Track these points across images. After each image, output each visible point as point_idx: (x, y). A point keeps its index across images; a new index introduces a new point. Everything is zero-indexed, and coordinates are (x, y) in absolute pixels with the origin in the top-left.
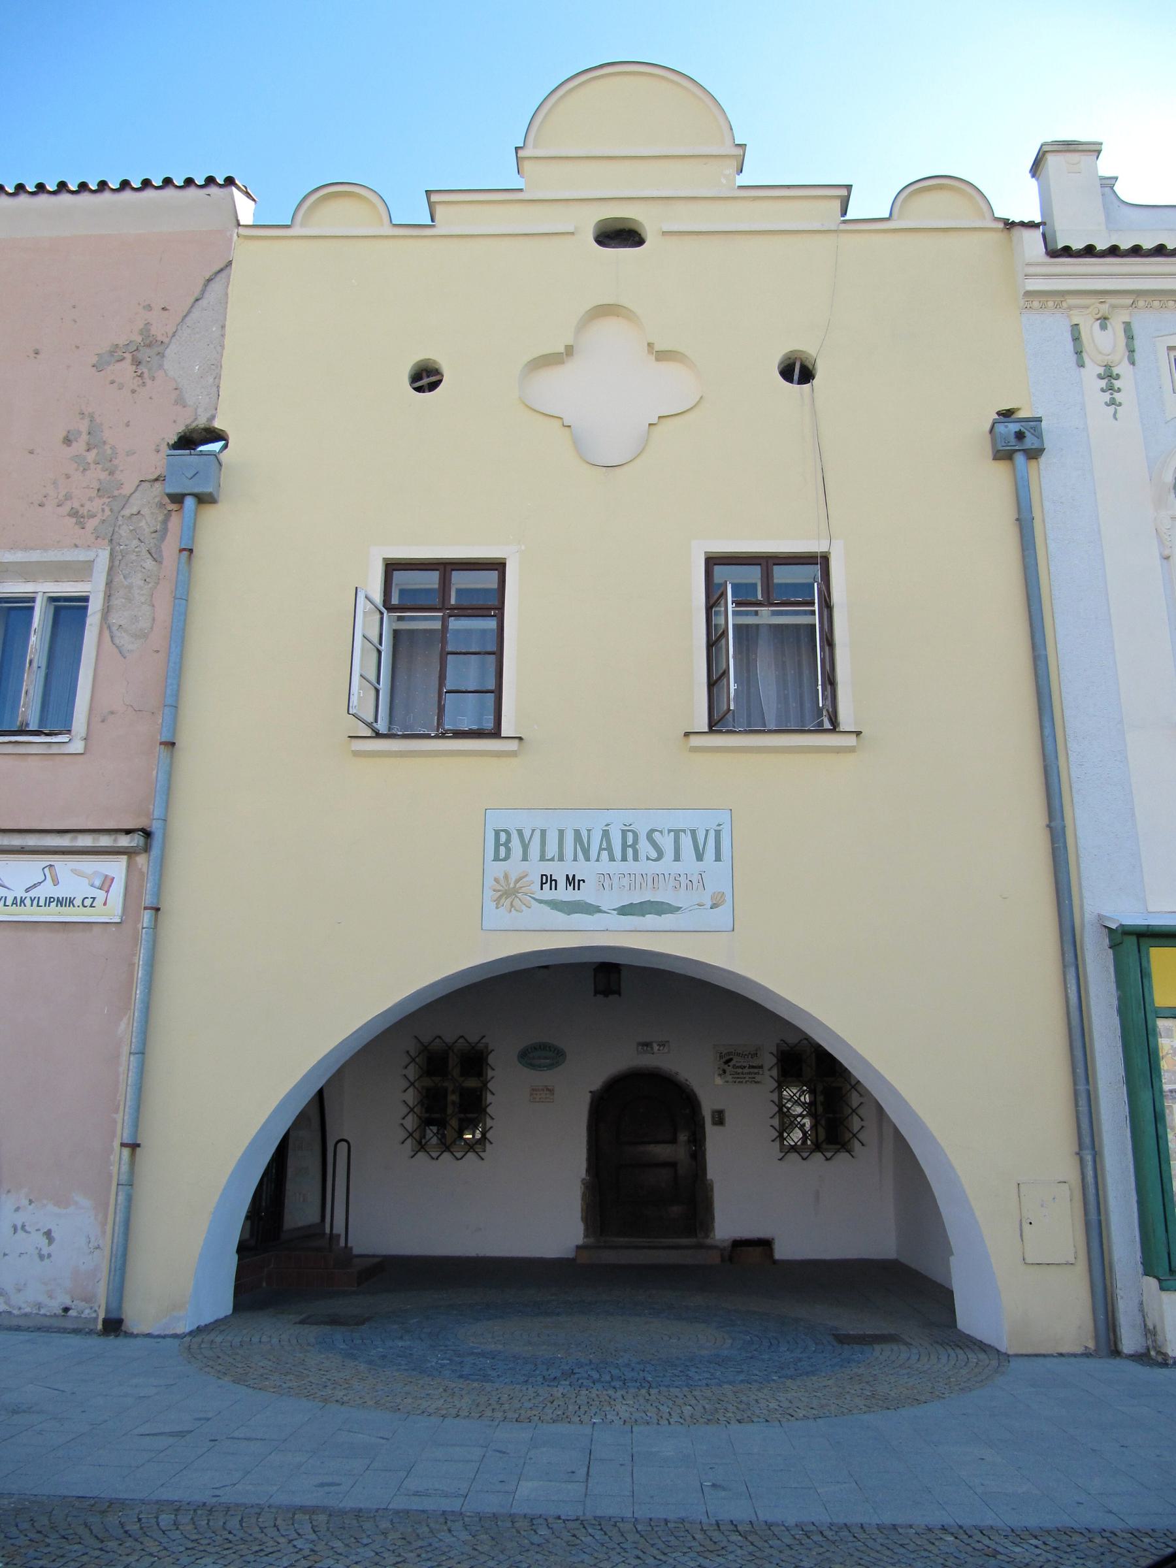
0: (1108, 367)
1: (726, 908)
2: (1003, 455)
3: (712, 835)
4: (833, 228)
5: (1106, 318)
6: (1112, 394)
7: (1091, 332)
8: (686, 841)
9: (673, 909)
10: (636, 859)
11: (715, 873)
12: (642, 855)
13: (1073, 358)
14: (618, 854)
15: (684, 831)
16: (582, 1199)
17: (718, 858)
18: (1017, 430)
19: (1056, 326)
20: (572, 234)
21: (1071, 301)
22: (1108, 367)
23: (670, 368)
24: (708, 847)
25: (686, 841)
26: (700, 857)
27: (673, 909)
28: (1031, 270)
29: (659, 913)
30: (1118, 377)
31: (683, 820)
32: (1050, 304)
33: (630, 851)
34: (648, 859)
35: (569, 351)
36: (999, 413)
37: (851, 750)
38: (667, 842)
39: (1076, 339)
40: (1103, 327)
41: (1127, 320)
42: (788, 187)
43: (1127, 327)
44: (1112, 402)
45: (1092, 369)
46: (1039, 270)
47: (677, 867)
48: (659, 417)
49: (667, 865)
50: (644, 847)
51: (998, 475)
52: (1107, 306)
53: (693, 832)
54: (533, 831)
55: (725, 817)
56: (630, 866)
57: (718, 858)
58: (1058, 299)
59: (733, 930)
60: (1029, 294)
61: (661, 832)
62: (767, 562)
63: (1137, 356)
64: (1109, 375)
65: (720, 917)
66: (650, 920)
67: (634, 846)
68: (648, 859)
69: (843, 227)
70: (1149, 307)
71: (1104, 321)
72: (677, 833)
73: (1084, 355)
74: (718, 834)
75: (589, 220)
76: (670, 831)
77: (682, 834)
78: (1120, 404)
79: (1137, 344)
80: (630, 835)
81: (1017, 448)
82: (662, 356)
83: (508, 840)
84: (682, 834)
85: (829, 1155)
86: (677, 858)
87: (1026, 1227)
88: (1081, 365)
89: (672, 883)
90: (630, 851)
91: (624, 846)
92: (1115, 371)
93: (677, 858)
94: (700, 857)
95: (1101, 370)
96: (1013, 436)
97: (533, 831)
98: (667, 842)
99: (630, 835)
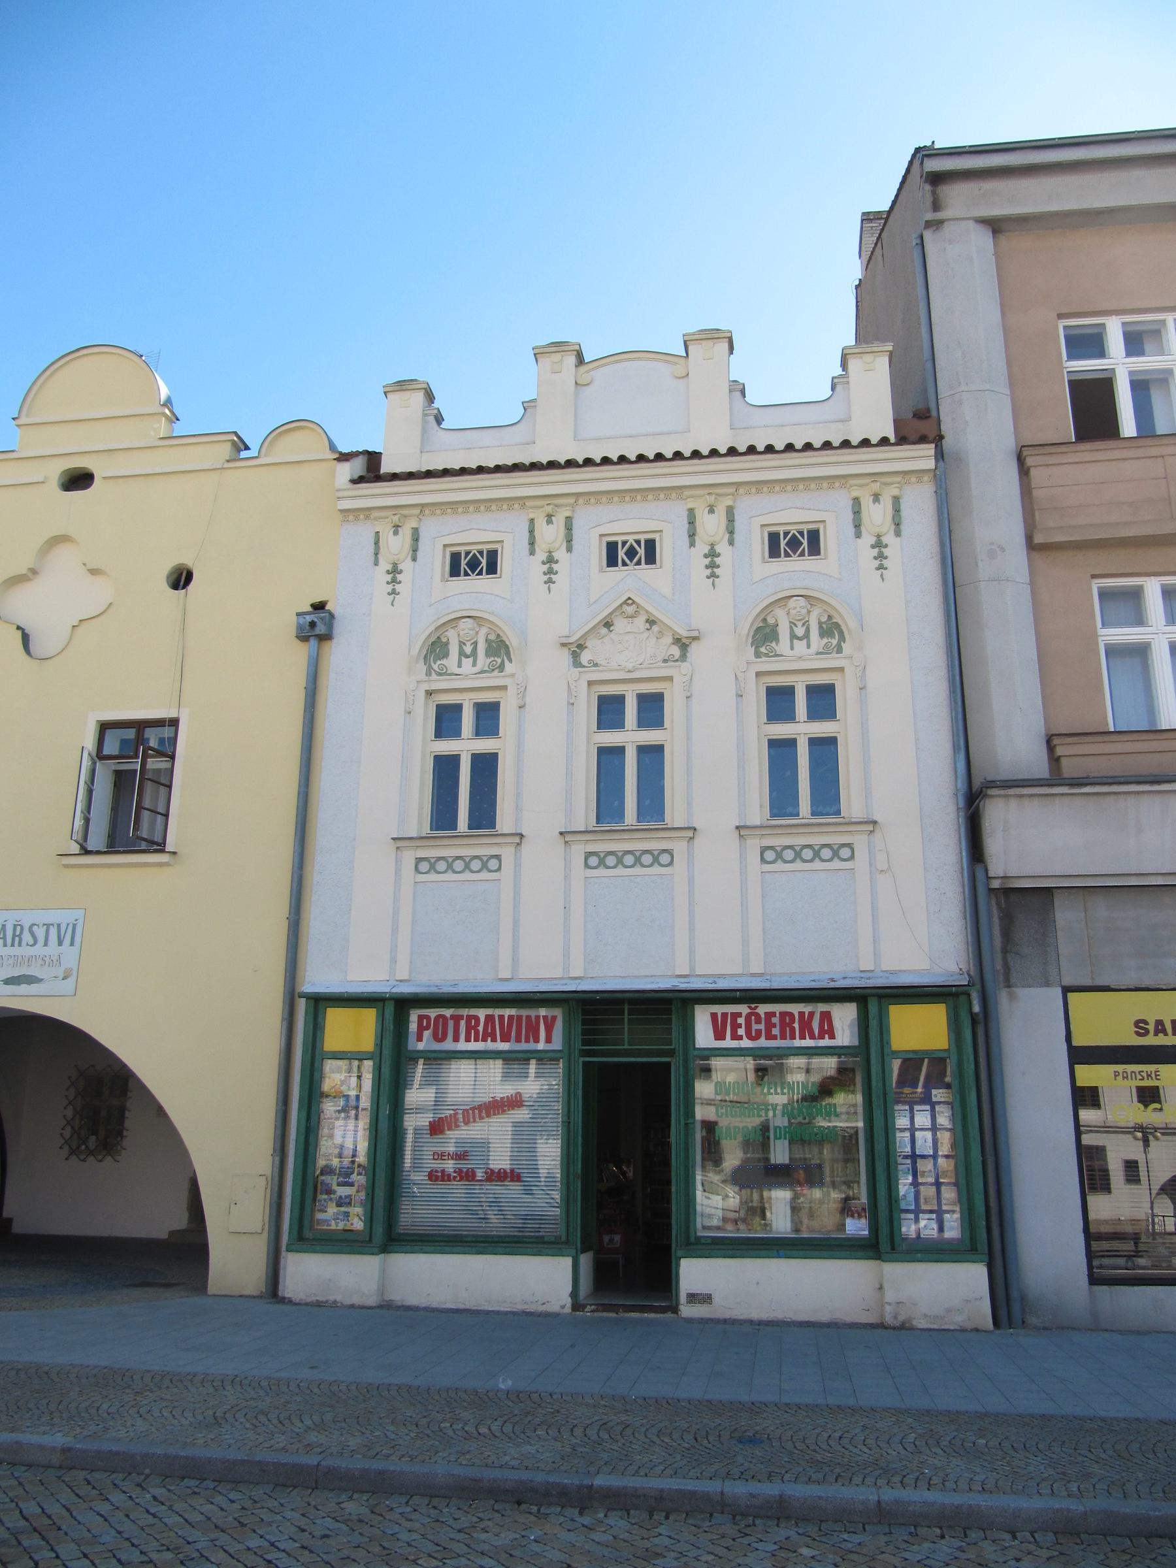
0: (395, 565)
1: (70, 982)
2: (303, 638)
3: (70, 928)
4: (219, 466)
5: (398, 526)
6: (881, 561)
7: (541, 527)
8: (53, 932)
9: (37, 980)
10: (20, 945)
11: (69, 955)
12: (24, 943)
13: (852, 530)
14: (9, 942)
15: (53, 925)
16: (189, 1192)
17: (72, 944)
18: (310, 620)
19: (363, 533)
20: (43, 482)
21: (375, 514)
22: (395, 565)
23: (98, 580)
24: (66, 938)
25: (53, 932)
26: (60, 943)
27: (37, 980)
28: (340, 494)
29: (29, 983)
30: (719, 555)
31: (53, 917)
32: (362, 517)
33: (17, 939)
34: (28, 945)
35: (34, 572)
36: (312, 605)
37: (167, 864)
38: (40, 933)
39: (692, 522)
40: (396, 533)
41: (415, 526)
42: (194, 436)
43: (896, 500)
44: (394, 592)
45: (868, 539)
46: (345, 494)
47: (46, 951)
48: (80, 621)
49: (39, 950)
50: (27, 937)
51: (300, 654)
52: (878, 484)
53: (59, 925)
54: (68, 924)
55: (79, 914)
56: (16, 950)
57: (72, 944)
58: (843, 481)
59: (75, 995)
60: (342, 511)
61: (38, 925)
62: (140, 725)
63: (420, 554)
64: (879, 544)
65: (69, 985)
66: (24, 989)
67: (20, 936)
68: (28, 945)
69: (227, 465)
70: (433, 514)
71: (876, 498)
72: (48, 926)
73: (696, 538)
74: (74, 926)
75: (56, 470)
76: (44, 925)
77: (51, 927)
78: (718, 577)
79: (421, 543)
80: (19, 928)
81: (309, 634)
82: (94, 572)
83: (21, 932)
84: (51, 927)
85: (100, 1157)
86: (46, 944)
87: (233, 1206)
88: (376, 564)
89: (40, 962)
90: (17, 939)
91: (14, 936)
92: (400, 567)
93: (46, 944)
94: (60, 943)
95: (390, 567)
96: (308, 624)
97: (68, 924)
98: (40, 933)
99: (19, 928)
